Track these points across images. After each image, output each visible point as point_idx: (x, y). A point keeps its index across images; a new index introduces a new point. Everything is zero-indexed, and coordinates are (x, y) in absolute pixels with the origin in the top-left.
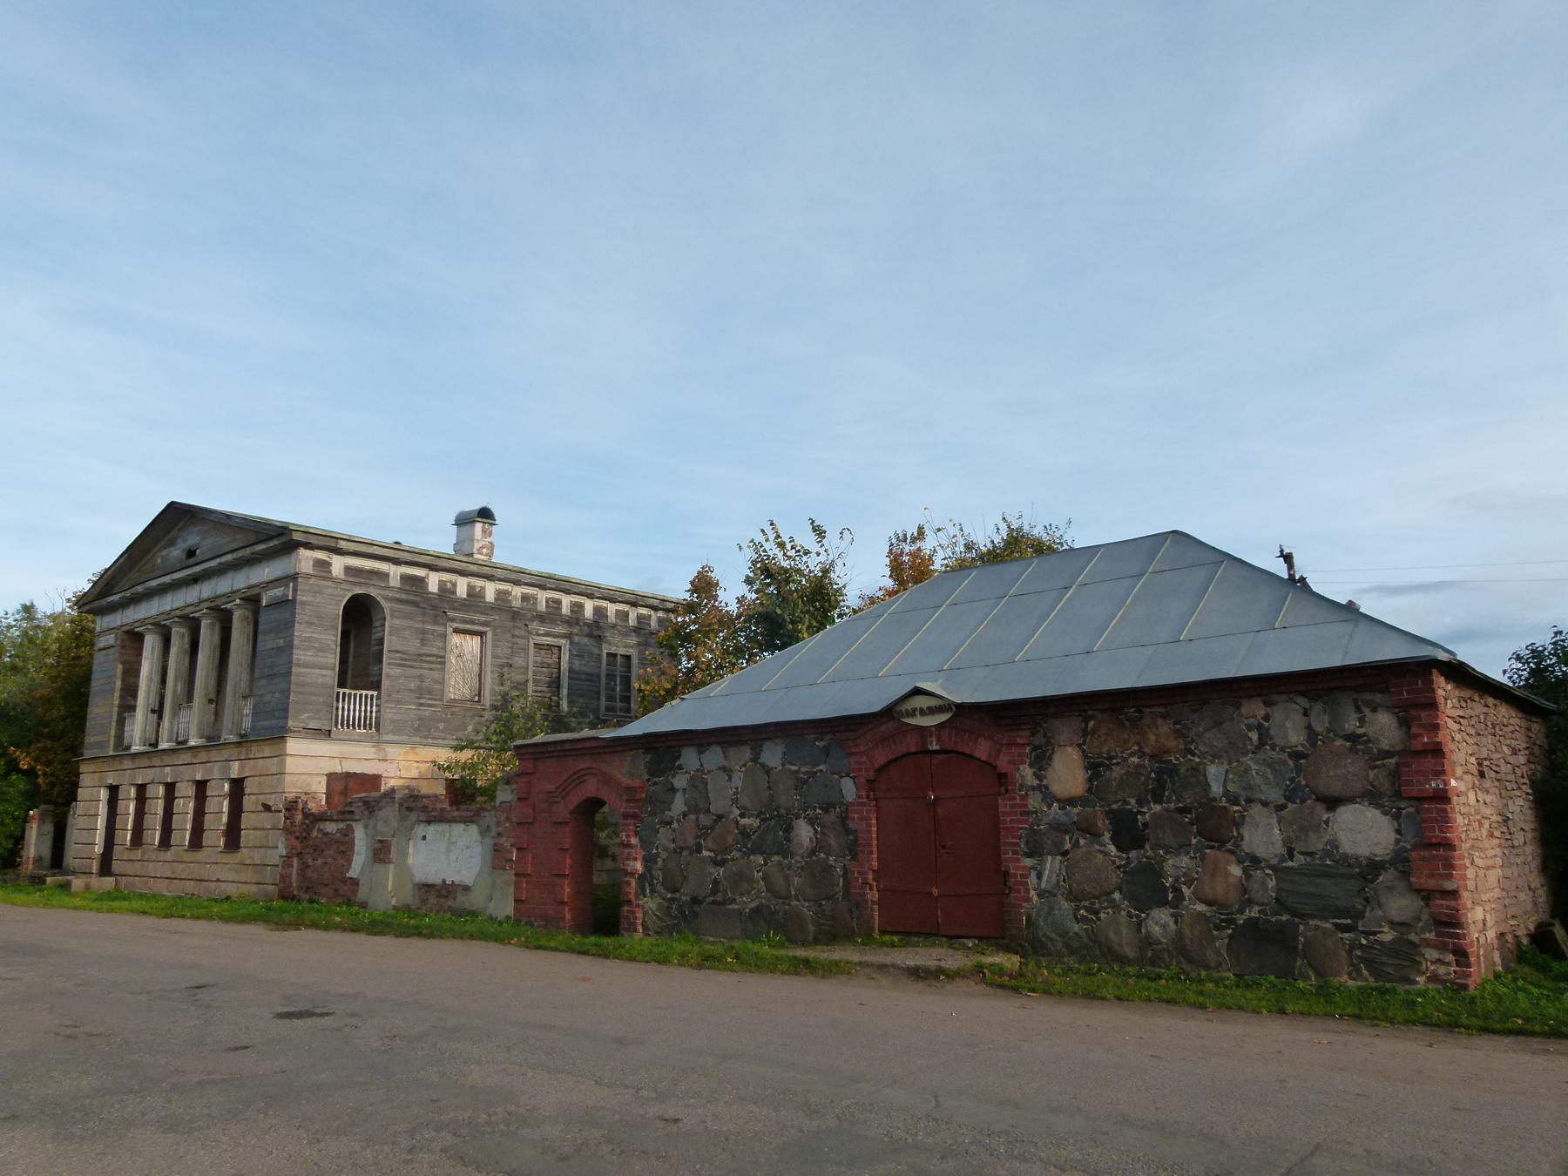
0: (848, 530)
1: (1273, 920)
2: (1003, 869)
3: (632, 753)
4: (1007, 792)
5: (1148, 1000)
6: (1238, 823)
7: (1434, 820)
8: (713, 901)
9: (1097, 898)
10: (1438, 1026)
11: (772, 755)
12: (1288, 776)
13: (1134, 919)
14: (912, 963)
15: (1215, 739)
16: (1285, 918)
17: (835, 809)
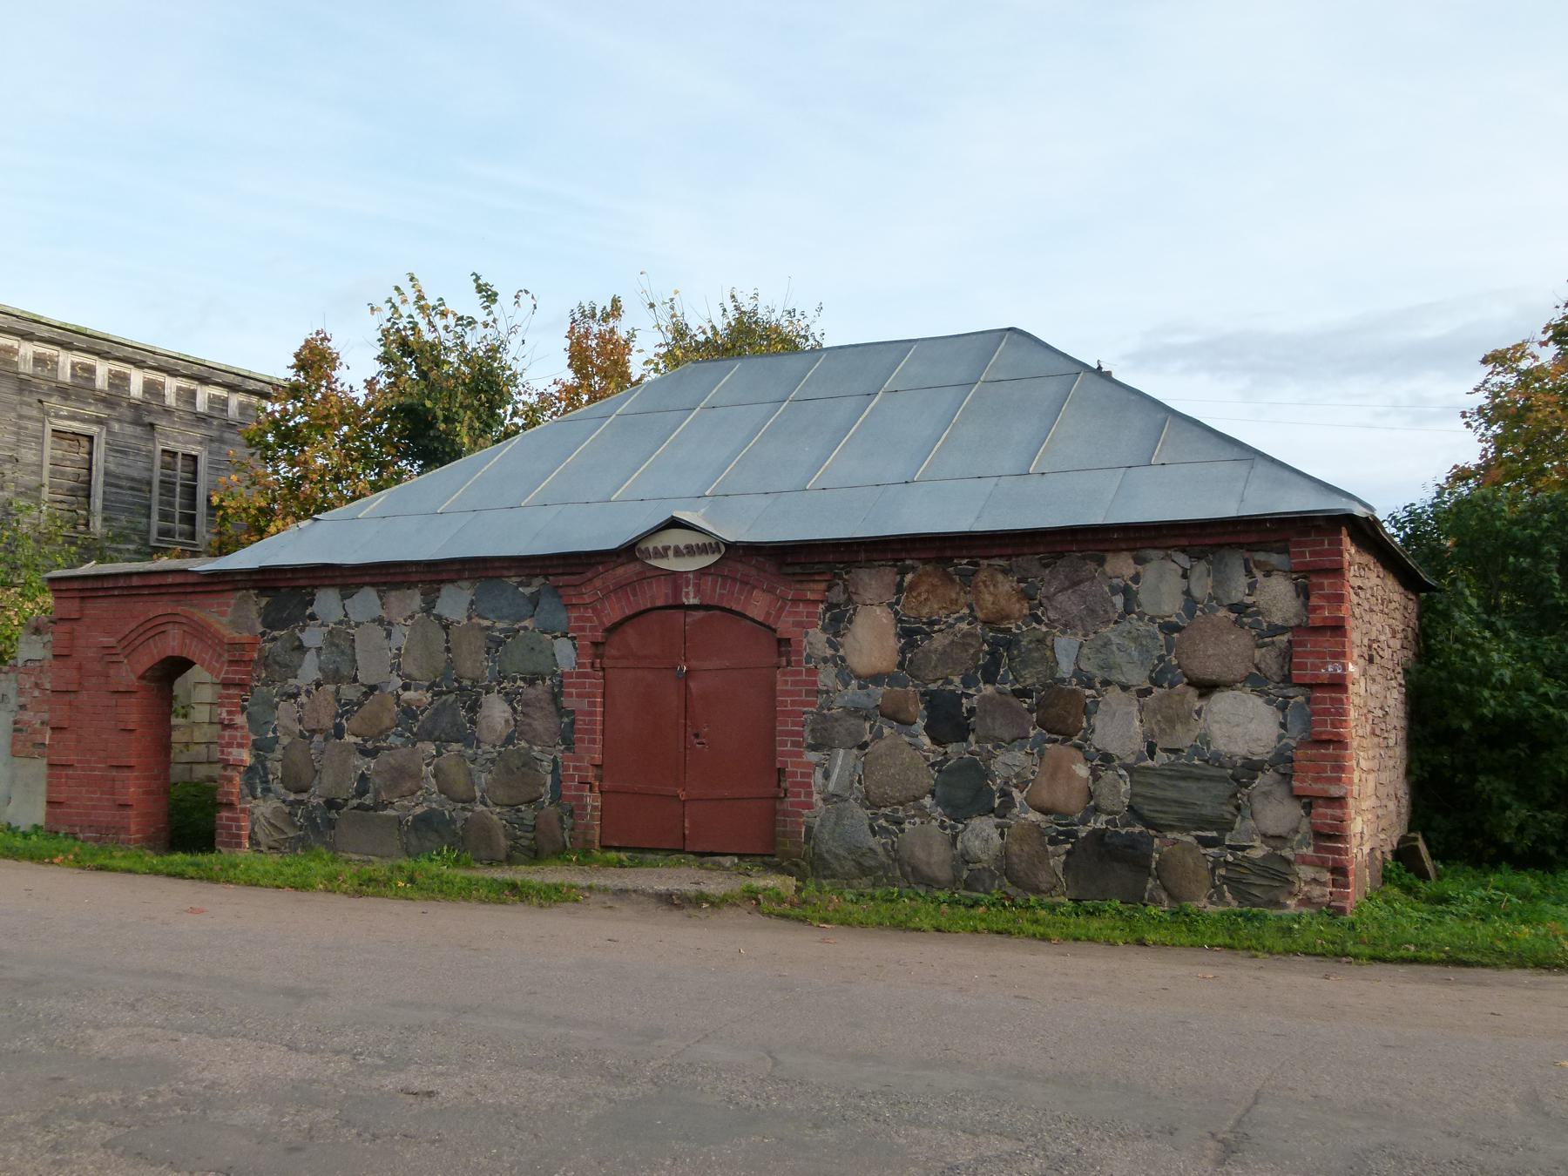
0: (527, 292)
1: (1123, 832)
2: (778, 766)
3: (239, 594)
4: (789, 663)
5: (975, 931)
6: (1088, 712)
7: (1326, 712)
8: (359, 804)
9: (901, 804)
10: (1323, 955)
11: (454, 602)
12: (1157, 653)
13: (948, 831)
14: (661, 887)
15: (1068, 602)
16: (1138, 829)
17: (544, 680)
